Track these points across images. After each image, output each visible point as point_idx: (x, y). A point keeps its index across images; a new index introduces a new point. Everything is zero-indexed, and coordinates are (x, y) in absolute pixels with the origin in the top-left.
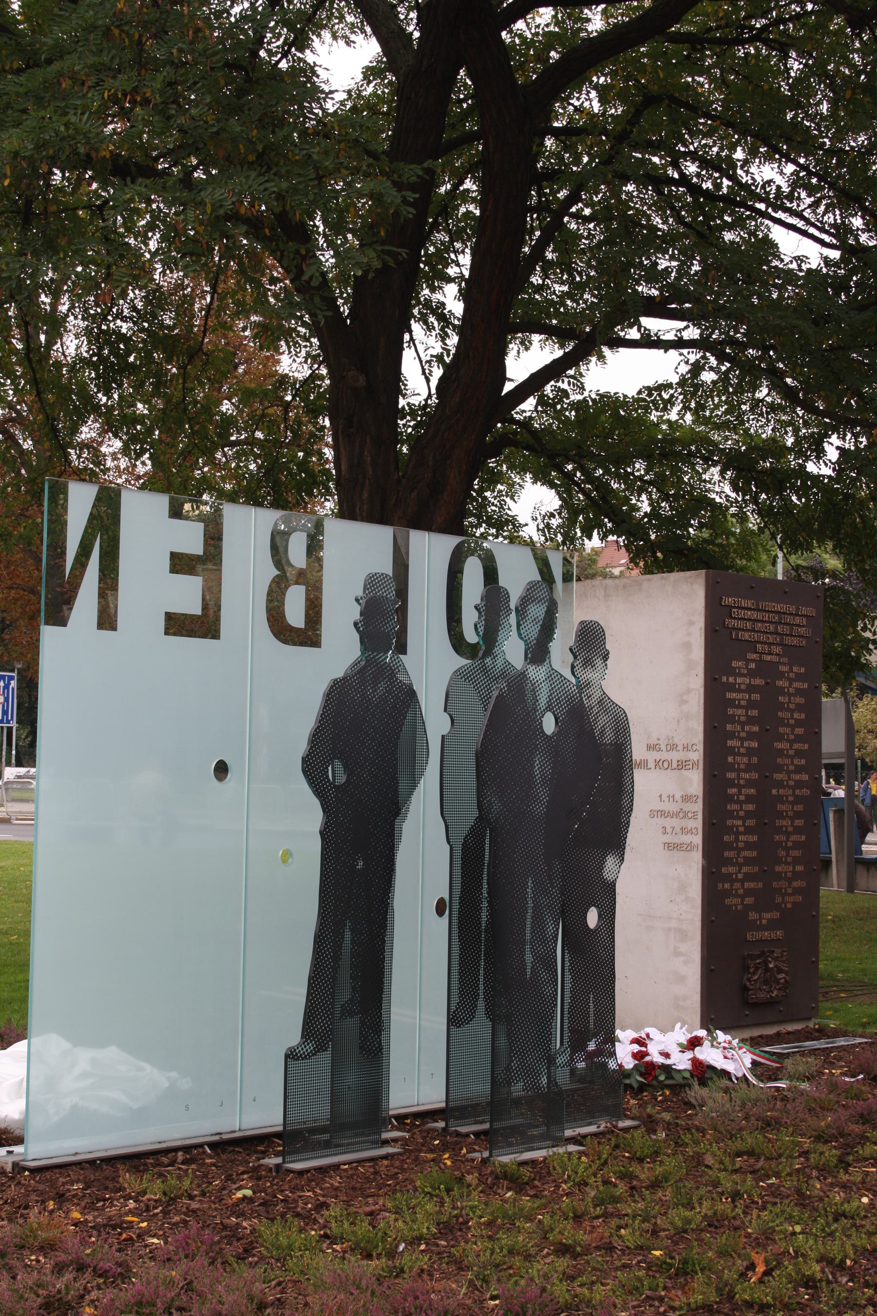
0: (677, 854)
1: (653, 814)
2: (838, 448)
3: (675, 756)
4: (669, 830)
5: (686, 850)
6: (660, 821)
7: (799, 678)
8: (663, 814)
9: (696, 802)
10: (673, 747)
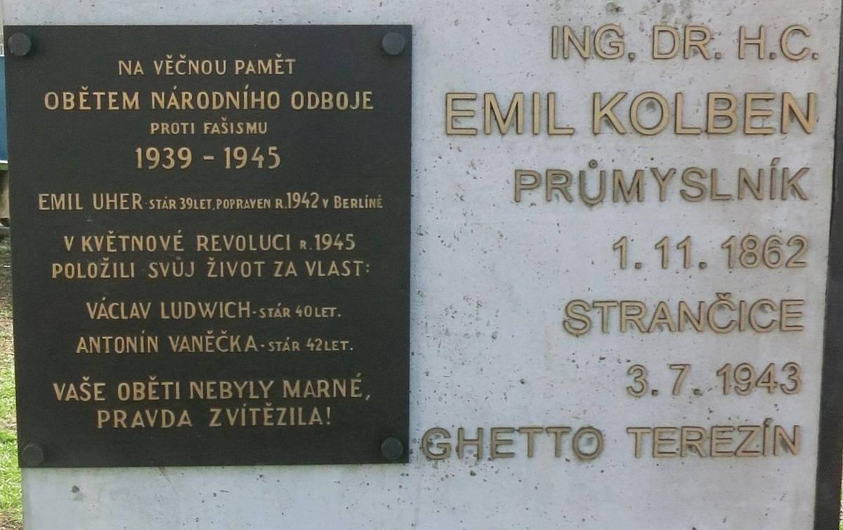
0: (700, 474)
2: (751, 121)
4: (661, 378)
5: (742, 452)
6: (621, 345)
8: (632, 314)
9: (453, 99)
10: (694, 42)
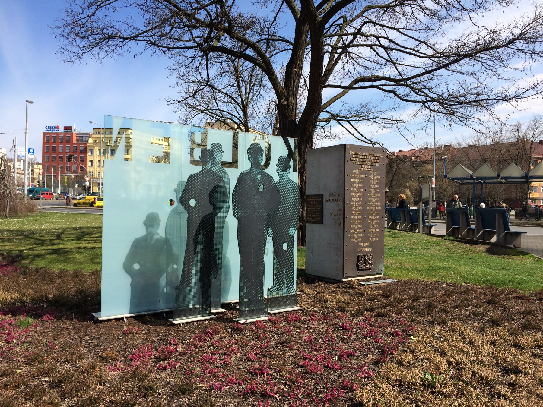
1: (331, 214)
3: (337, 198)
7: (377, 175)
